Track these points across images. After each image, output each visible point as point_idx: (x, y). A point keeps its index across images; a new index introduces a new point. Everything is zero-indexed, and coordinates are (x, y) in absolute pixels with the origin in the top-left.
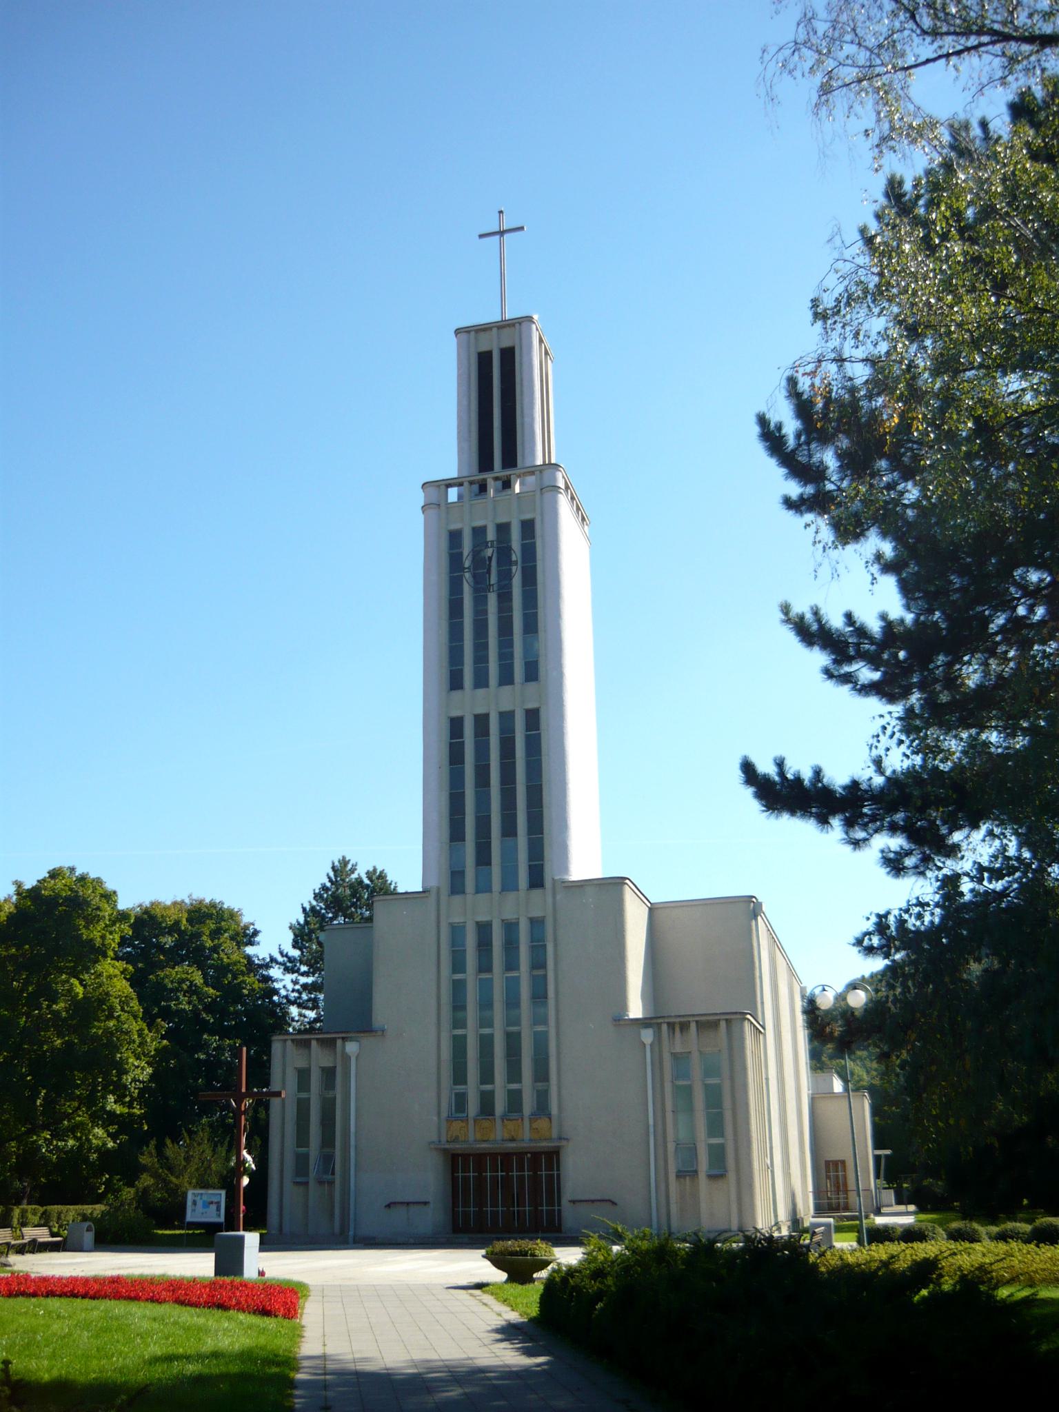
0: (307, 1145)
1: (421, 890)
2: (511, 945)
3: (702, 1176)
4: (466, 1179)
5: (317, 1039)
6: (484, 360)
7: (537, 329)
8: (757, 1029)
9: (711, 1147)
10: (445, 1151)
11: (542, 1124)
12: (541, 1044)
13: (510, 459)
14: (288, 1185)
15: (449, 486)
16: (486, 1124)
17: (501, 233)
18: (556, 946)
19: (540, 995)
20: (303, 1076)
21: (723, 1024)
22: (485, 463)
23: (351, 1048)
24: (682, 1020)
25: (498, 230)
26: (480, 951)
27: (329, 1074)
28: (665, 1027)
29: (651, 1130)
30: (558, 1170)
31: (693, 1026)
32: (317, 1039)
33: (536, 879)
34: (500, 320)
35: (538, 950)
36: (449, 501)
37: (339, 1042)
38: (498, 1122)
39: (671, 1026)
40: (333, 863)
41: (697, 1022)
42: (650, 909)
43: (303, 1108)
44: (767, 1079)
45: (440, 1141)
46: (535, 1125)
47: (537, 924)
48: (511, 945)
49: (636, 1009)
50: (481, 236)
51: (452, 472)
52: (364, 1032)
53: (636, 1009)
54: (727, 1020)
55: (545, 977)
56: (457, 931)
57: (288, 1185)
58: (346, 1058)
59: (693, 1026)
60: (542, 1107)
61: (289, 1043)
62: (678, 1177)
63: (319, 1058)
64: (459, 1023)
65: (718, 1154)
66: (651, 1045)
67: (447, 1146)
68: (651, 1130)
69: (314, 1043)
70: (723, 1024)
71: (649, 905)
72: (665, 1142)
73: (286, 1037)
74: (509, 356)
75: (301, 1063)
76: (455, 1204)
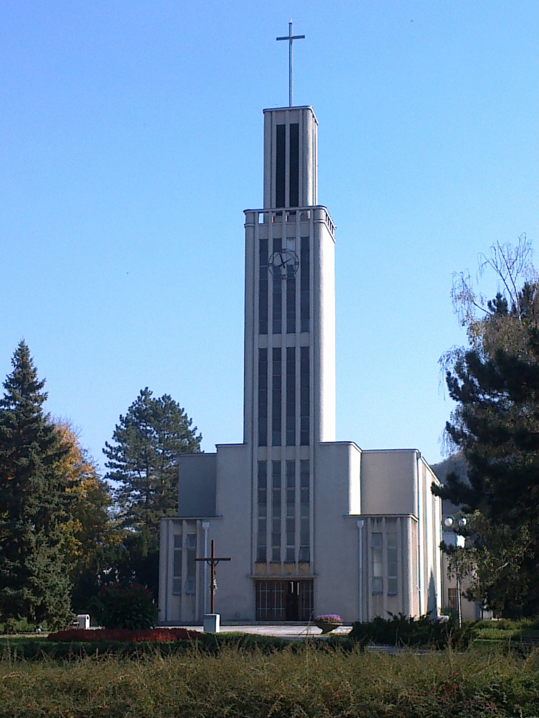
0: (180, 575)
1: (242, 443)
2: (291, 474)
3: (385, 595)
4: (264, 593)
5: (186, 520)
6: (281, 129)
7: (313, 116)
8: (414, 520)
9: (390, 580)
10: (254, 579)
11: (305, 566)
12: (305, 524)
13: (294, 202)
14: (170, 595)
15: (259, 213)
16: (276, 566)
17: (291, 38)
18: (314, 475)
19: (305, 500)
20: (178, 540)
21: (399, 519)
22: (280, 202)
23: (206, 525)
24: (378, 516)
25: (288, 35)
26: (259, 505)
27: (192, 538)
28: (369, 520)
29: (361, 571)
30: (312, 607)
31: (384, 520)
32: (186, 520)
33: (305, 442)
34: (288, 106)
35: (305, 475)
36: (260, 222)
37: (198, 522)
38: (282, 564)
39: (373, 519)
40: (449, 374)
41: (386, 518)
42: (361, 454)
43: (178, 556)
44: (419, 546)
45: (252, 574)
46: (301, 567)
47: (305, 463)
48: (291, 474)
49: (355, 509)
50: (278, 39)
51: (260, 206)
52: (213, 516)
53: (355, 509)
54: (400, 518)
55: (308, 491)
56: (262, 465)
57: (170, 595)
58: (202, 531)
59: (384, 520)
60: (305, 560)
61: (171, 522)
62: (373, 595)
63: (187, 529)
64: (263, 513)
65: (393, 585)
66: (362, 529)
67: (256, 577)
68: (361, 571)
69: (184, 523)
70: (399, 519)
71: (361, 451)
72: (368, 578)
73: (169, 518)
74: (295, 128)
75: (177, 533)
76: (257, 606)
